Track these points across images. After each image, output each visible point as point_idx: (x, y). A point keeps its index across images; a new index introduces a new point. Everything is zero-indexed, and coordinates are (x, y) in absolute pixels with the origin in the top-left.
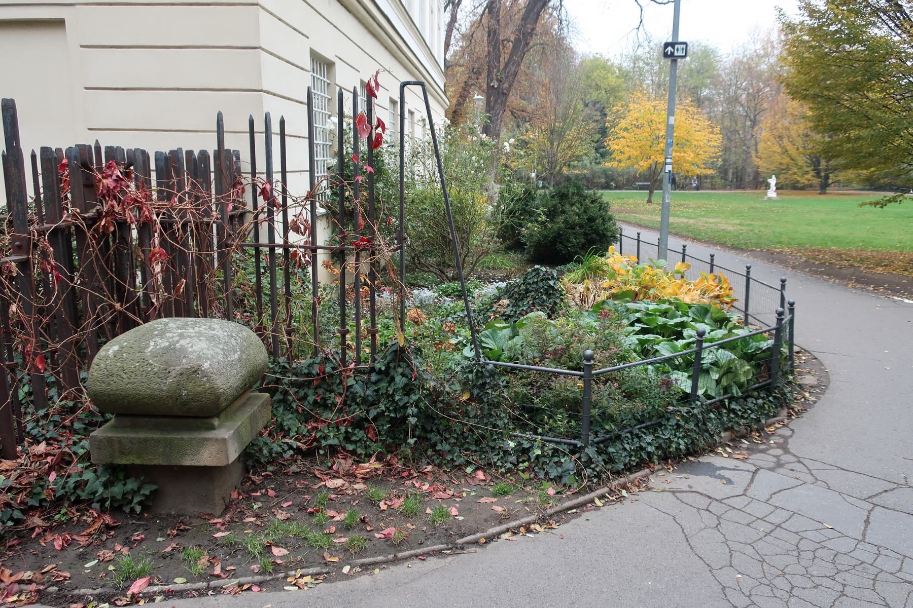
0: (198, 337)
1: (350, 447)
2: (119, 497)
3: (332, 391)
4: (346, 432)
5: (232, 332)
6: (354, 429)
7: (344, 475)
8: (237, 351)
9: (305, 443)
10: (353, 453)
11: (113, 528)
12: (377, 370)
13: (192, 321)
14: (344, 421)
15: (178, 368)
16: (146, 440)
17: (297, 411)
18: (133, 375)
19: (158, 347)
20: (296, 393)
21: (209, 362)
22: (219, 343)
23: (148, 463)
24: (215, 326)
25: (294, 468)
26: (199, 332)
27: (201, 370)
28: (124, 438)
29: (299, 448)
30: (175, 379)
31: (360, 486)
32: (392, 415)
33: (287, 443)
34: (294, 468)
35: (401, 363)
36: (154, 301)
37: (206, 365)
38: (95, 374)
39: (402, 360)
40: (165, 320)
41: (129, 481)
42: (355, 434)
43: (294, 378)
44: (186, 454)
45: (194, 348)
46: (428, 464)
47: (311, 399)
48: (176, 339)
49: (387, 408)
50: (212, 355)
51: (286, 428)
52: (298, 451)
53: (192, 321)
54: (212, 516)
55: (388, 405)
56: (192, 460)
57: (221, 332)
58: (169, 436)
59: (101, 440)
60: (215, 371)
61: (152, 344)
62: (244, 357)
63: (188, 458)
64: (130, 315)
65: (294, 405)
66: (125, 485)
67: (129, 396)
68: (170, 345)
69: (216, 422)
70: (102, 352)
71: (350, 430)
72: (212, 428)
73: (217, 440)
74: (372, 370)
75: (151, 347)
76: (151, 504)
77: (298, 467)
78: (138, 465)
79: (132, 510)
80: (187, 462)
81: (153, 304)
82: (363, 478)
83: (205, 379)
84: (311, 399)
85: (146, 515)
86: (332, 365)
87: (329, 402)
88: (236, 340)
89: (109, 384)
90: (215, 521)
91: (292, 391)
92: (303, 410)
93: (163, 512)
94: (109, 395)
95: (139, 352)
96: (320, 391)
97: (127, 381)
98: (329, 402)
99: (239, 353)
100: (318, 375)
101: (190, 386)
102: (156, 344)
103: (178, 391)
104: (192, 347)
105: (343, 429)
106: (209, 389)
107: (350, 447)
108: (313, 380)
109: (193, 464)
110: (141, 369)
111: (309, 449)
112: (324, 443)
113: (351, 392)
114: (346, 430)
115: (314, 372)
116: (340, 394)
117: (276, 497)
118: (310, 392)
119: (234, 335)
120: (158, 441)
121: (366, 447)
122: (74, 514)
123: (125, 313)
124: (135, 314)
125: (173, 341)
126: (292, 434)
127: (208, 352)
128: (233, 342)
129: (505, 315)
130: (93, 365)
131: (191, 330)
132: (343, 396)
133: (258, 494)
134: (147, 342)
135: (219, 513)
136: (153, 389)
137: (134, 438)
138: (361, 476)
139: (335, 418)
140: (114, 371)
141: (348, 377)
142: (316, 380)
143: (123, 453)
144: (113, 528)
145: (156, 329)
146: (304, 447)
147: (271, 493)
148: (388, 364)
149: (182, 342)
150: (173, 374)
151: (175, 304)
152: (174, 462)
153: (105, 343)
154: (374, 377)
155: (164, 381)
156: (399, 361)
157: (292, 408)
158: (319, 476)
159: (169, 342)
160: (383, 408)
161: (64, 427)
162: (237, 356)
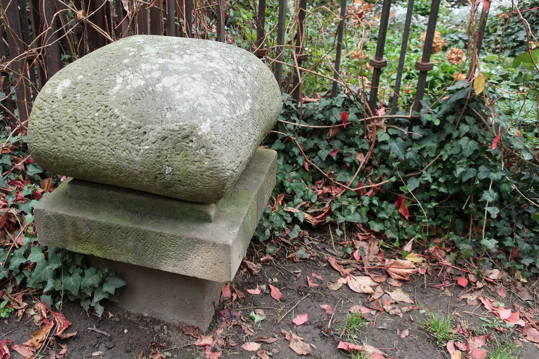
0: (191, 73)
1: (377, 227)
2: (75, 292)
3: (352, 145)
4: (371, 204)
5: (237, 64)
6: (381, 200)
7: (370, 270)
8: (247, 98)
9: (314, 214)
10: (380, 235)
11: (66, 341)
12: (424, 124)
13: (178, 43)
14: (368, 189)
15: (158, 128)
16: (110, 228)
17: (303, 167)
18: (90, 131)
19: (128, 87)
20: (304, 144)
21: (209, 121)
22: (223, 85)
23: (113, 258)
24: (213, 54)
25: (301, 252)
26: (190, 64)
27: (197, 136)
28: (80, 219)
29: (306, 222)
30: (154, 147)
31: (398, 295)
32: (442, 190)
33: (292, 214)
34: (301, 252)
35: (467, 118)
36: (126, 8)
37: (204, 128)
38: (37, 122)
39: (469, 112)
40: (139, 39)
41: (88, 272)
42: (383, 209)
43: (303, 125)
44: (167, 256)
45: (185, 93)
46: (493, 267)
47: (324, 153)
48: (156, 74)
49: (435, 179)
50: (213, 108)
51: (289, 190)
52: (305, 225)
53: (178, 43)
54: (198, 332)
55: (436, 175)
56: (175, 266)
57: (223, 64)
58: (143, 227)
59: (48, 217)
60: (219, 139)
61: (119, 80)
62: (257, 107)
63: (170, 262)
64: (95, 26)
65: (300, 160)
66: (82, 275)
67: (85, 163)
68: (147, 86)
69: (212, 211)
70: (47, 89)
71: (375, 202)
72: (207, 219)
73: (215, 245)
74: (415, 121)
75: (118, 87)
76: (117, 301)
77: (307, 251)
78: (98, 258)
79: (92, 309)
80: (168, 267)
81: (125, 12)
82: (400, 280)
83: (202, 152)
84: (324, 153)
85: (111, 315)
86: (356, 110)
87: (347, 160)
88: (244, 77)
89: (55, 141)
90: (203, 343)
91: (300, 140)
92: (311, 167)
93: (133, 311)
94: (56, 158)
95: (100, 93)
96: (337, 144)
97: (80, 139)
98: (347, 160)
99: (250, 101)
100: (338, 123)
101: (177, 160)
102: (125, 82)
103: (158, 166)
104: (181, 91)
105: (366, 201)
106: (209, 169)
107: (377, 227)
108: (328, 129)
109: (176, 272)
110: (102, 123)
111: (319, 224)
112: (341, 219)
113: (380, 151)
114: (371, 201)
115: (332, 119)
116: (364, 151)
117: (283, 300)
118: (323, 144)
119: (241, 69)
120: (127, 232)
121: (399, 229)
122: (19, 305)
123: (89, 25)
124: (104, 29)
125: (151, 78)
126: (297, 200)
127: (208, 103)
128: (241, 81)
129: (517, 41)
130: (34, 109)
131: (178, 60)
132: (368, 154)
133: (257, 291)
134: (112, 77)
135: (205, 327)
136: (119, 158)
137: (93, 222)
138: (397, 277)
139: (356, 183)
140: (63, 121)
141: (378, 128)
142: (333, 129)
143: (78, 239)
144: (66, 341)
145: (125, 55)
146: (313, 221)
147: (276, 293)
148: (446, 114)
149: (166, 81)
150: (151, 136)
151: (151, 14)
152: (149, 264)
153: (70, 61)
154: (417, 133)
155: (136, 146)
156: (465, 114)
157: (296, 162)
158: (336, 268)
159: (146, 80)
160: (429, 178)
161: (15, 171)
162: (247, 107)
